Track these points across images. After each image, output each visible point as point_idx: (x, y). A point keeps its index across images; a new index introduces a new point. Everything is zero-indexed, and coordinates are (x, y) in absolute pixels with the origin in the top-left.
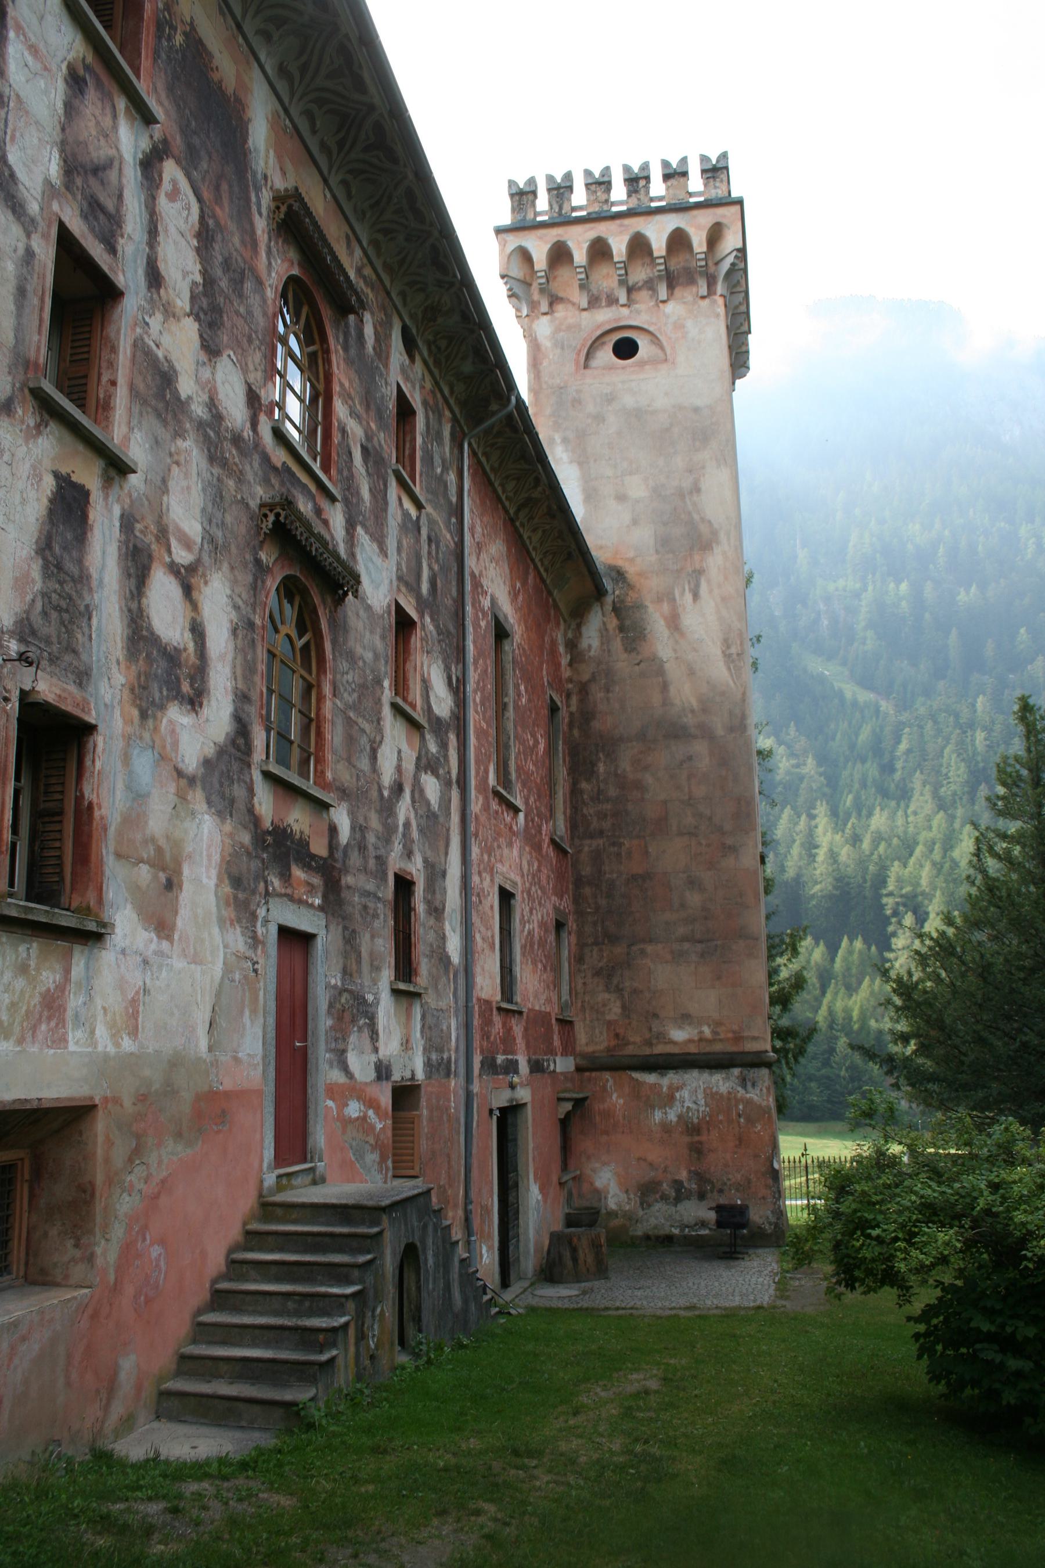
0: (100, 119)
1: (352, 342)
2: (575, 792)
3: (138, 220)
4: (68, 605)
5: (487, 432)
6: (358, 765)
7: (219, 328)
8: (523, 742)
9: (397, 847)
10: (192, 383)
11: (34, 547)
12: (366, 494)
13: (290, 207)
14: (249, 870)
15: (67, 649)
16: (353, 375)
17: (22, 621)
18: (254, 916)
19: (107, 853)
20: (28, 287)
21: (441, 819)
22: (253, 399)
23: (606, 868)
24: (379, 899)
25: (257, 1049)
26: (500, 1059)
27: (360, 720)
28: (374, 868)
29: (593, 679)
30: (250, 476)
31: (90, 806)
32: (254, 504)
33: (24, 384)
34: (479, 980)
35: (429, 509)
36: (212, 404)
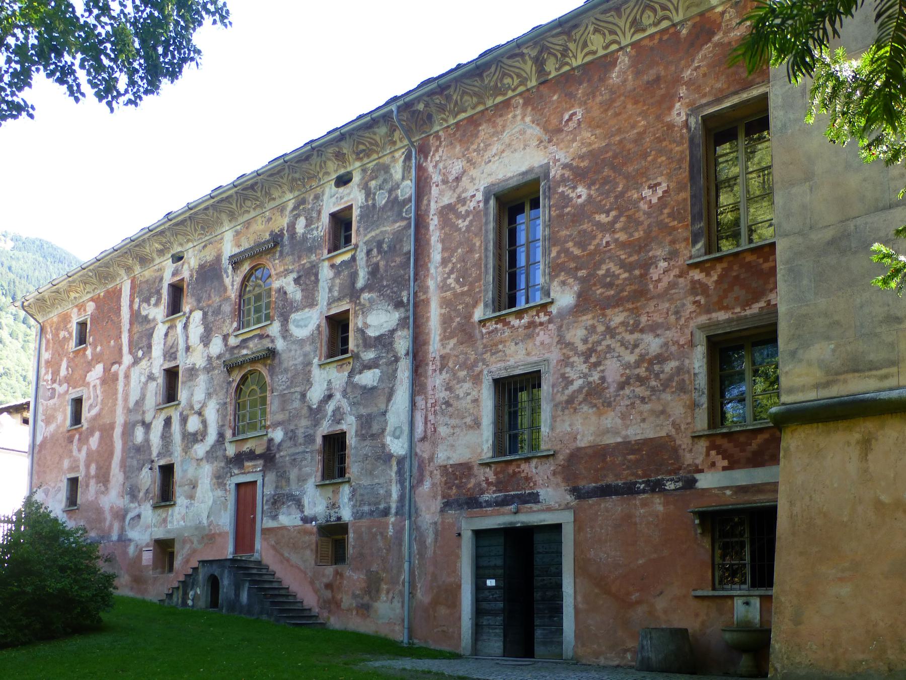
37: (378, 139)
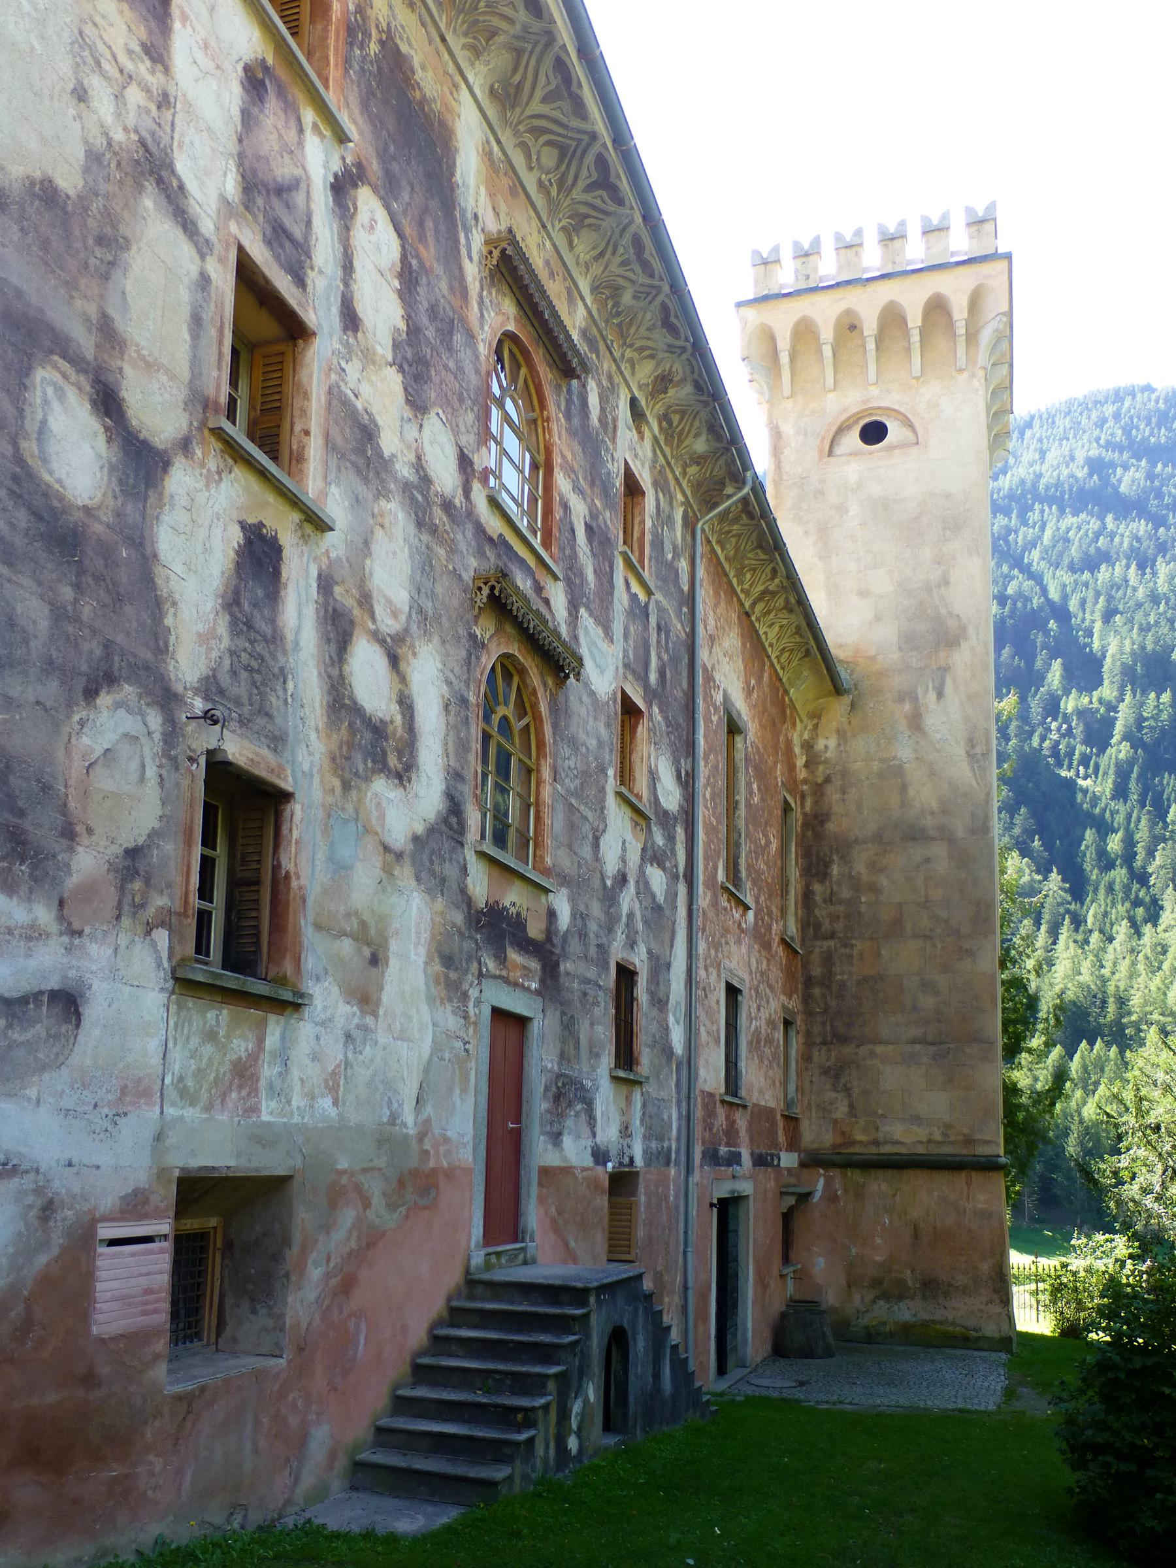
0: (283, 132)
1: (575, 410)
2: (807, 898)
3: (330, 251)
4: (260, 665)
5: (723, 516)
6: (580, 852)
7: (426, 383)
8: (755, 841)
9: (620, 938)
10: (396, 441)
11: (220, 601)
12: (590, 576)
13: (503, 251)
14: (461, 949)
15: (259, 712)
16: (578, 448)
17: (207, 678)
18: (465, 995)
19: (306, 923)
20: (204, 316)
21: (667, 912)
22: (464, 462)
23: (837, 969)
24: (600, 986)
25: (470, 1129)
26: (723, 1150)
27: (582, 808)
28: (595, 956)
29: (828, 780)
30: (463, 546)
31: (287, 876)
32: (467, 576)
33: (203, 423)
34: (702, 1073)
35: (658, 596)
36: (419, 464)
37: (686, 443)
